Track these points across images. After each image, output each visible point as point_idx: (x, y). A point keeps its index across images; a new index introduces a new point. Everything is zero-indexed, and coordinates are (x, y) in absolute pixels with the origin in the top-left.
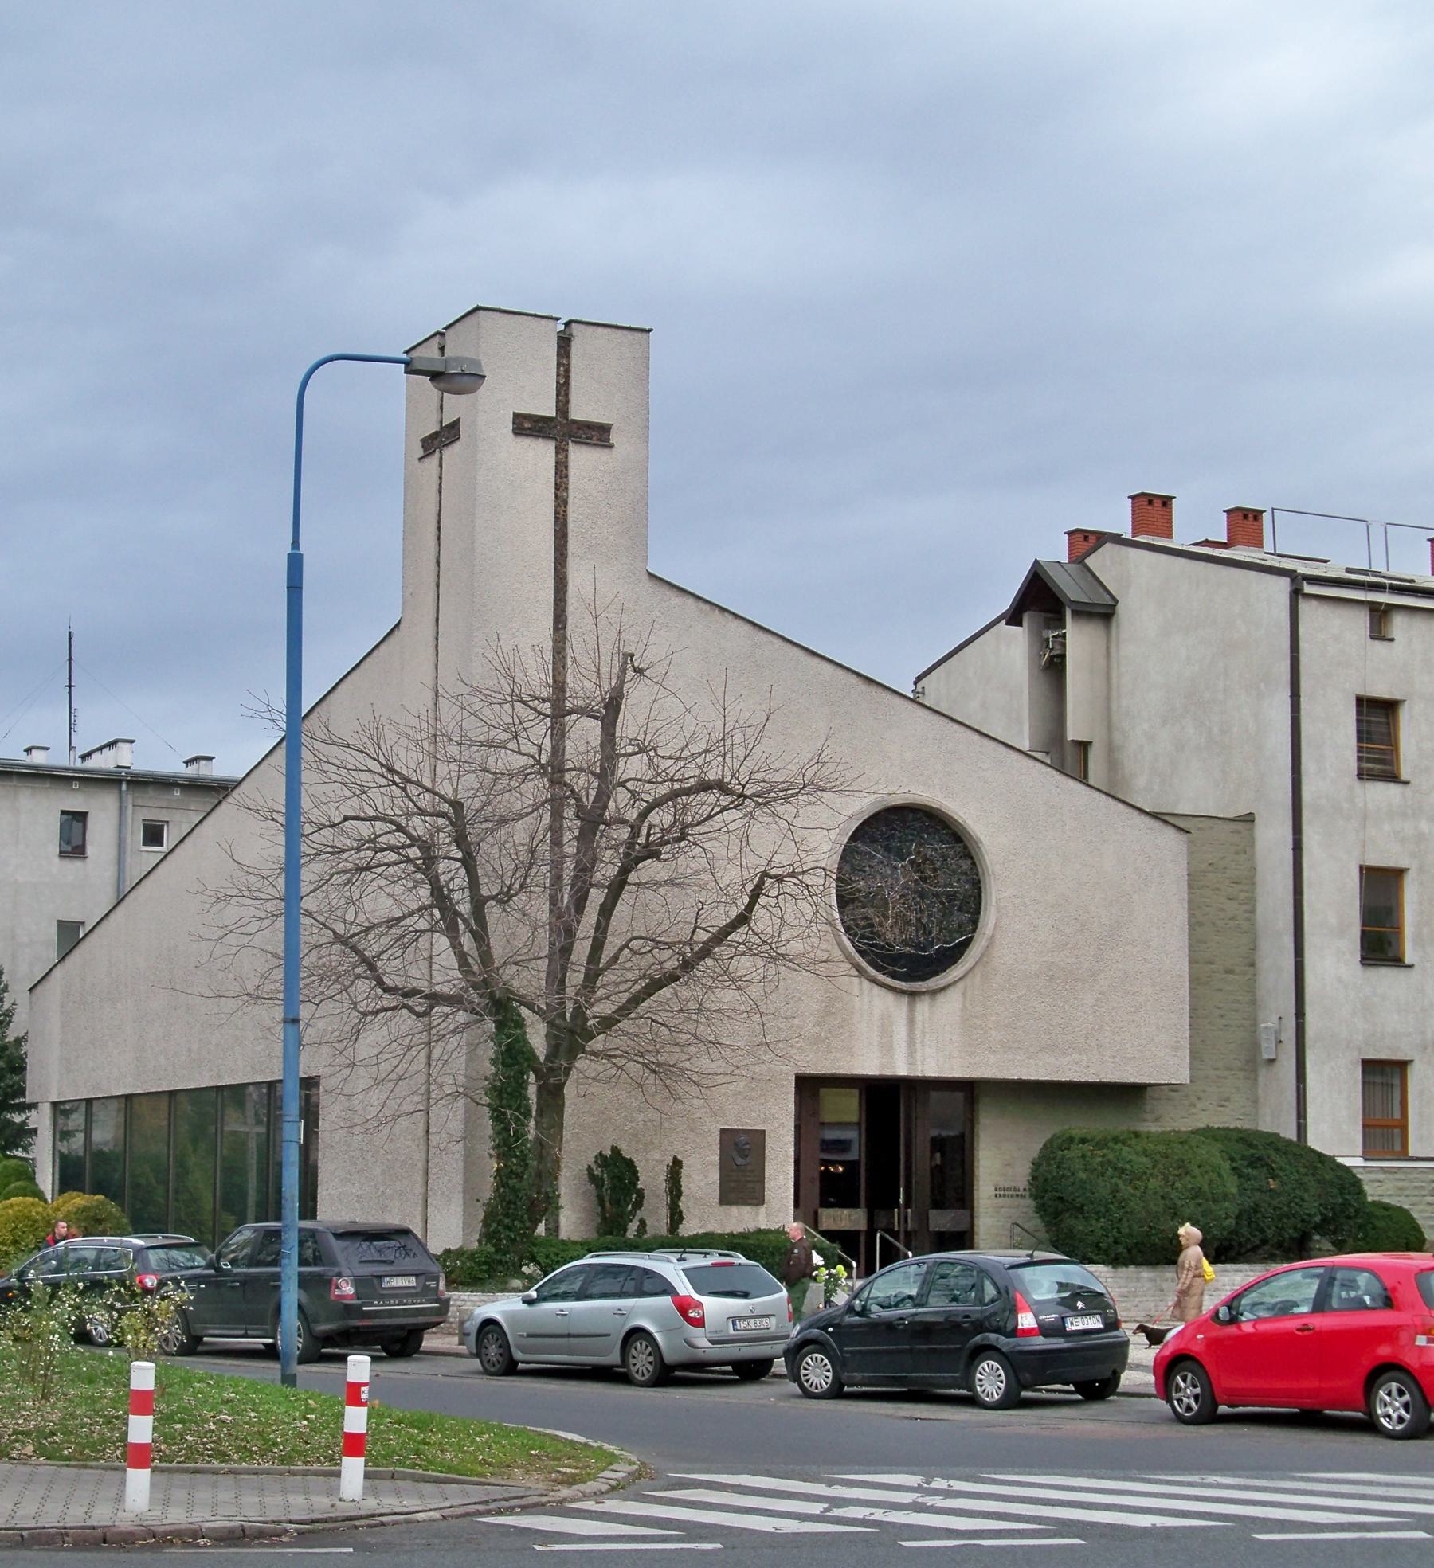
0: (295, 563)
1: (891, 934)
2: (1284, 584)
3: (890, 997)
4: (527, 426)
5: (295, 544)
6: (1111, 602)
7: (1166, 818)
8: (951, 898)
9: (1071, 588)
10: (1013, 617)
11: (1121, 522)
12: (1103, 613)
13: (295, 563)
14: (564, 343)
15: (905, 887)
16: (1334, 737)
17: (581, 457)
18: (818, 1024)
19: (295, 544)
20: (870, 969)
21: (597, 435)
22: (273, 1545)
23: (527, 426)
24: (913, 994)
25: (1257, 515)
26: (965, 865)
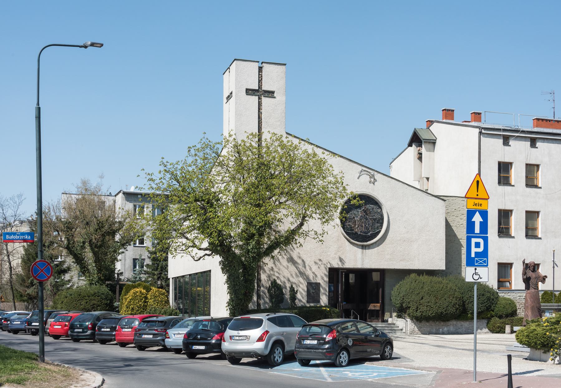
0: (39, 110)
1: (357, 230)
2: (477, 130)
3: (355, 248)
4: (270, 94)
5: (38, 104)
6: (435, 139)
7: (442, 197)
8: (375, 220)
9: (423, 135)
10: (410, 145)
11: (439, 116)
12: (433, 143)
13: (39, 110)
14: (260, 69)
15: (361, 216)
16: (491, 176)
17: (265, 100)
18: (335, 254)
19: (38, 104)
20: (365, 243)
21: (249, 92)
22: (144, 362)
23: (270, 94)
24: (363, 247)
25: (480, 114)
26: (379, 210)
